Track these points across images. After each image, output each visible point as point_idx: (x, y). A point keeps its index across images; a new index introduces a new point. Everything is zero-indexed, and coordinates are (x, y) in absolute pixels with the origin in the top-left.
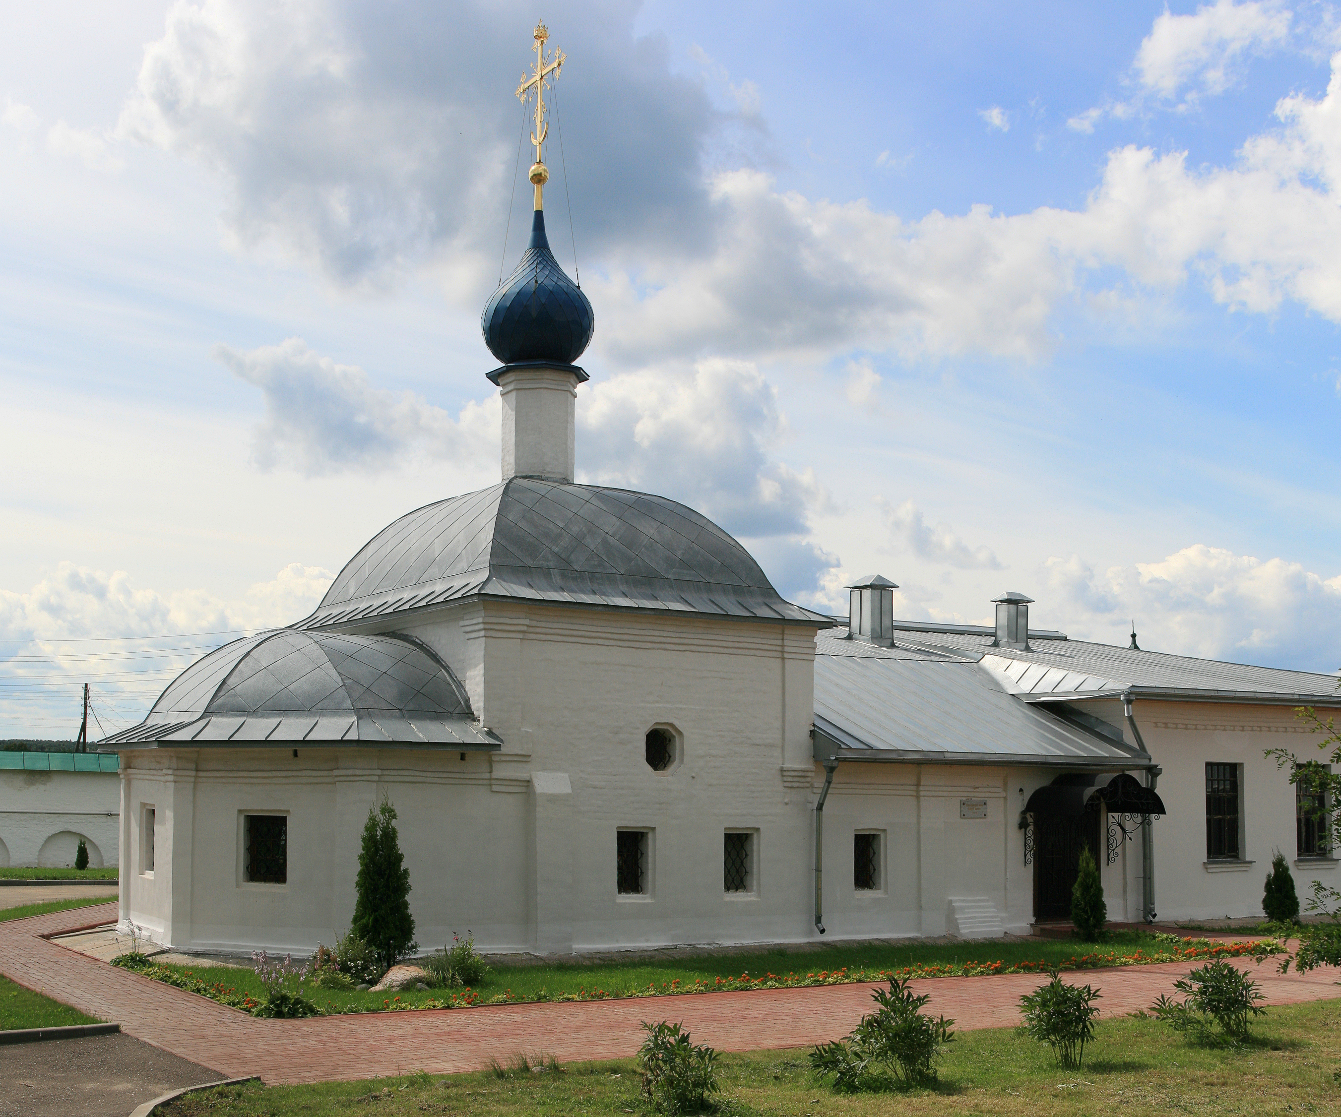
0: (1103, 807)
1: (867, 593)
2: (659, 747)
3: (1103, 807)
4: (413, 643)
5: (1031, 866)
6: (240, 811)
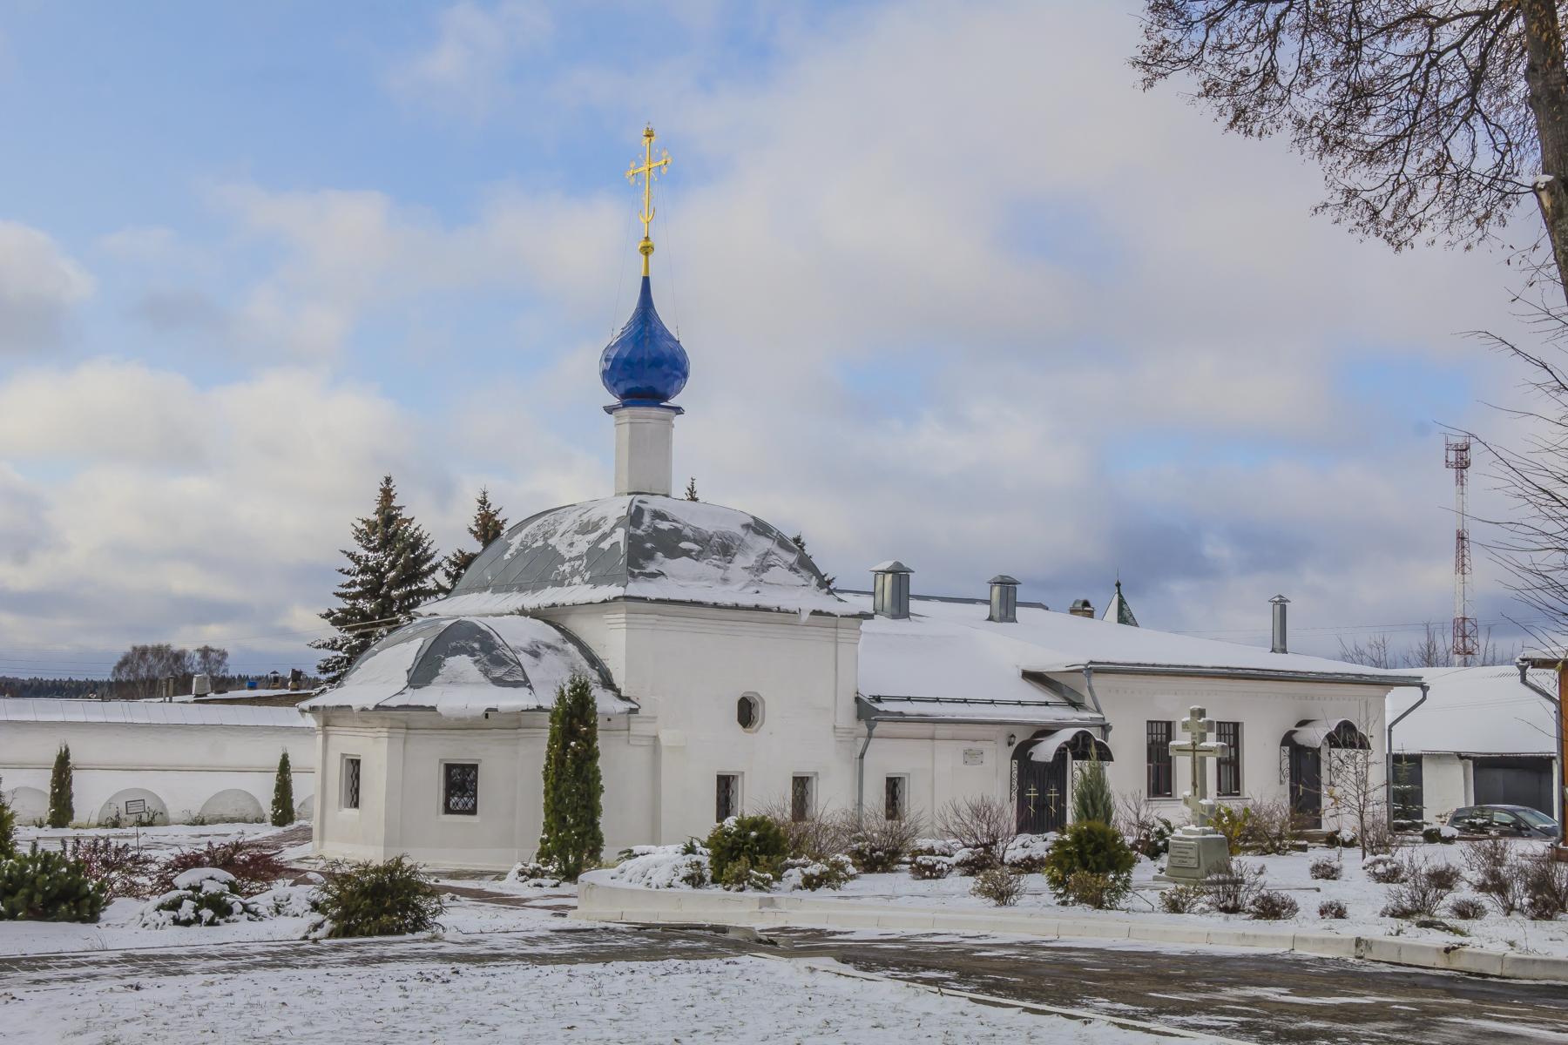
0: (1069, 755)
1: (889, 577)
2: (747, 712)
3: (1069, 755)
4: (557, 628)
6: (343, 755)
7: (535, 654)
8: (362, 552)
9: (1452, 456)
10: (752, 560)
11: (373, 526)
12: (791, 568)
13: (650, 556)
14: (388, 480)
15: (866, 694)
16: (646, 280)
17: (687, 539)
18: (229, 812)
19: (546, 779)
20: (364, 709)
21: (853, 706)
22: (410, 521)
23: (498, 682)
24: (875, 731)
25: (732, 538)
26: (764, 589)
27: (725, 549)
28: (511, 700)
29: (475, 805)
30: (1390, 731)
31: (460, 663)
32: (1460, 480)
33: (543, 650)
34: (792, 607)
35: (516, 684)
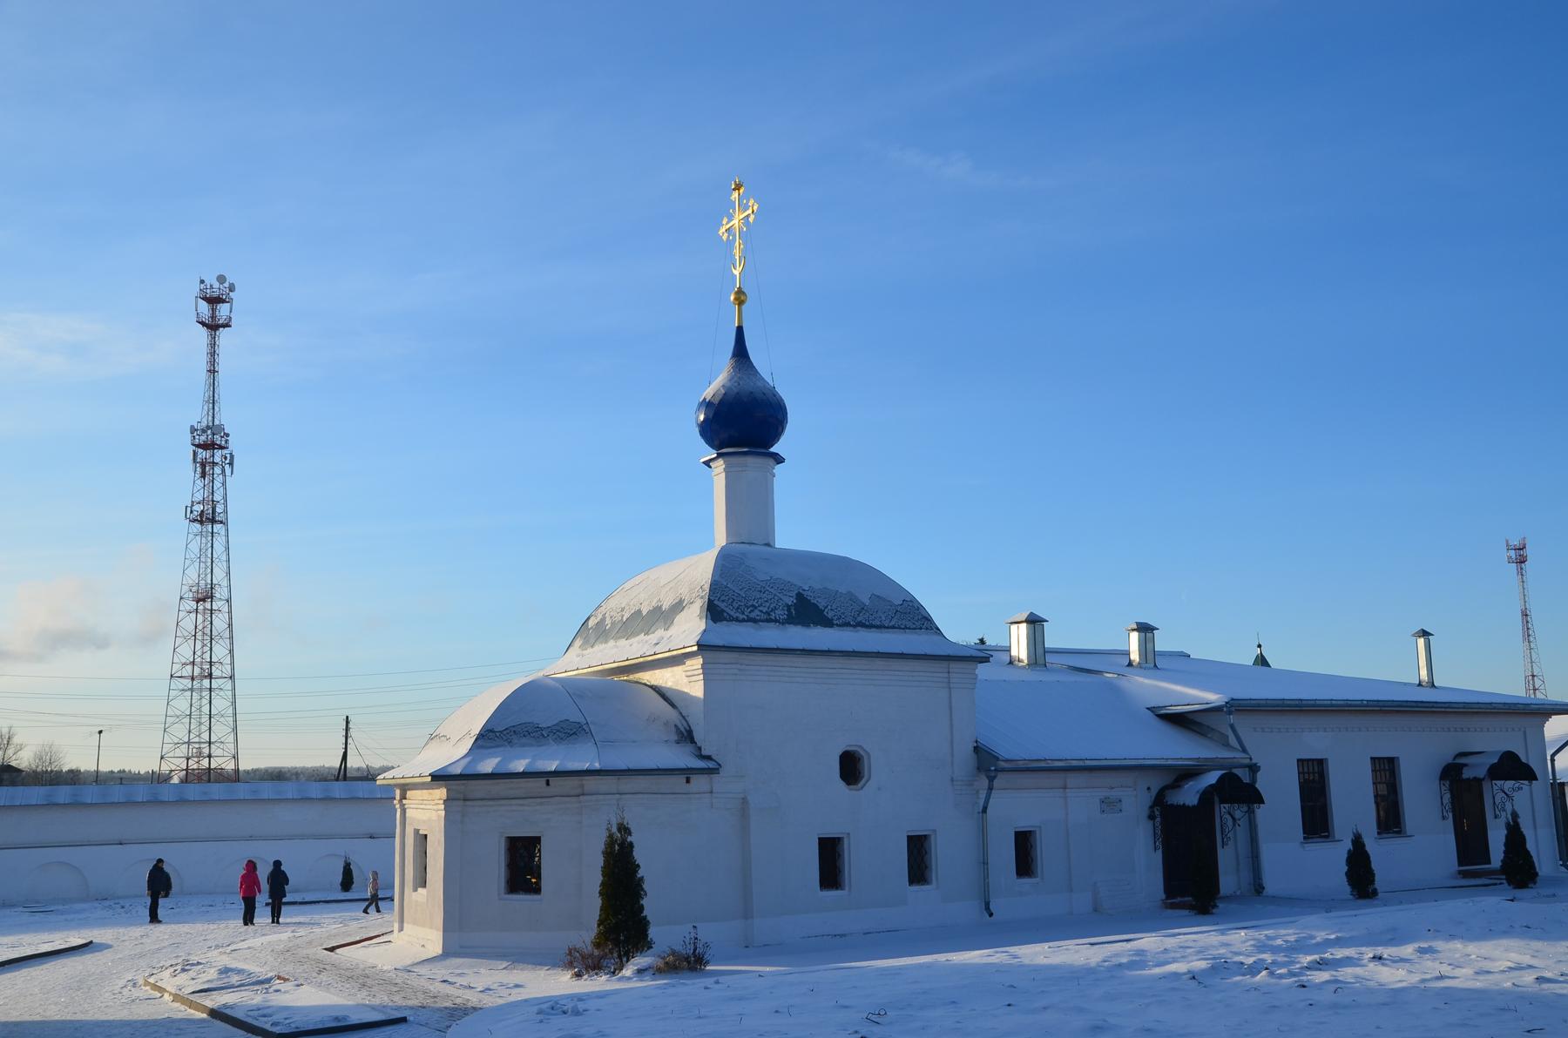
0: (1216, 799)
2: (851, 767)
3: (1216, 799)
5: (1160, 852)
16: (740, 330)
30: (1553, 761)
32: (1521, 572)
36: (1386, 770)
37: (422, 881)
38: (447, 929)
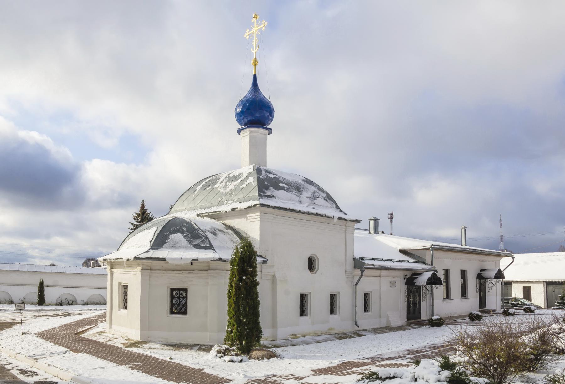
2: (311, 264)
6: (120, 284)
7: (214, 233)
8: (135, 223)
9: (389, 216)
10: (309, 194)
11: (139, 215)
12: (325, 199)
13: (267, 188)
14: (143, 201)
15: (357, 256)
16: (255, 76)
17: (282, 183)
18: (96, 301)
19: (229, 297)
20: (128, 260)
21: (352, 262)
22: (150, 213)
23: (197, 247)
24: (365, 273)
25: (300, 184)
26: (316, 208)
27: (298, 189)
28: (207, 255)
29: (186, 310)
31: (178, 237)
32: (391, 221)
33: (218, 232)
34: (331, 215)
35: (206, 248)
36: (464, 274)
37: (125, 305)
38: (142, 329)
